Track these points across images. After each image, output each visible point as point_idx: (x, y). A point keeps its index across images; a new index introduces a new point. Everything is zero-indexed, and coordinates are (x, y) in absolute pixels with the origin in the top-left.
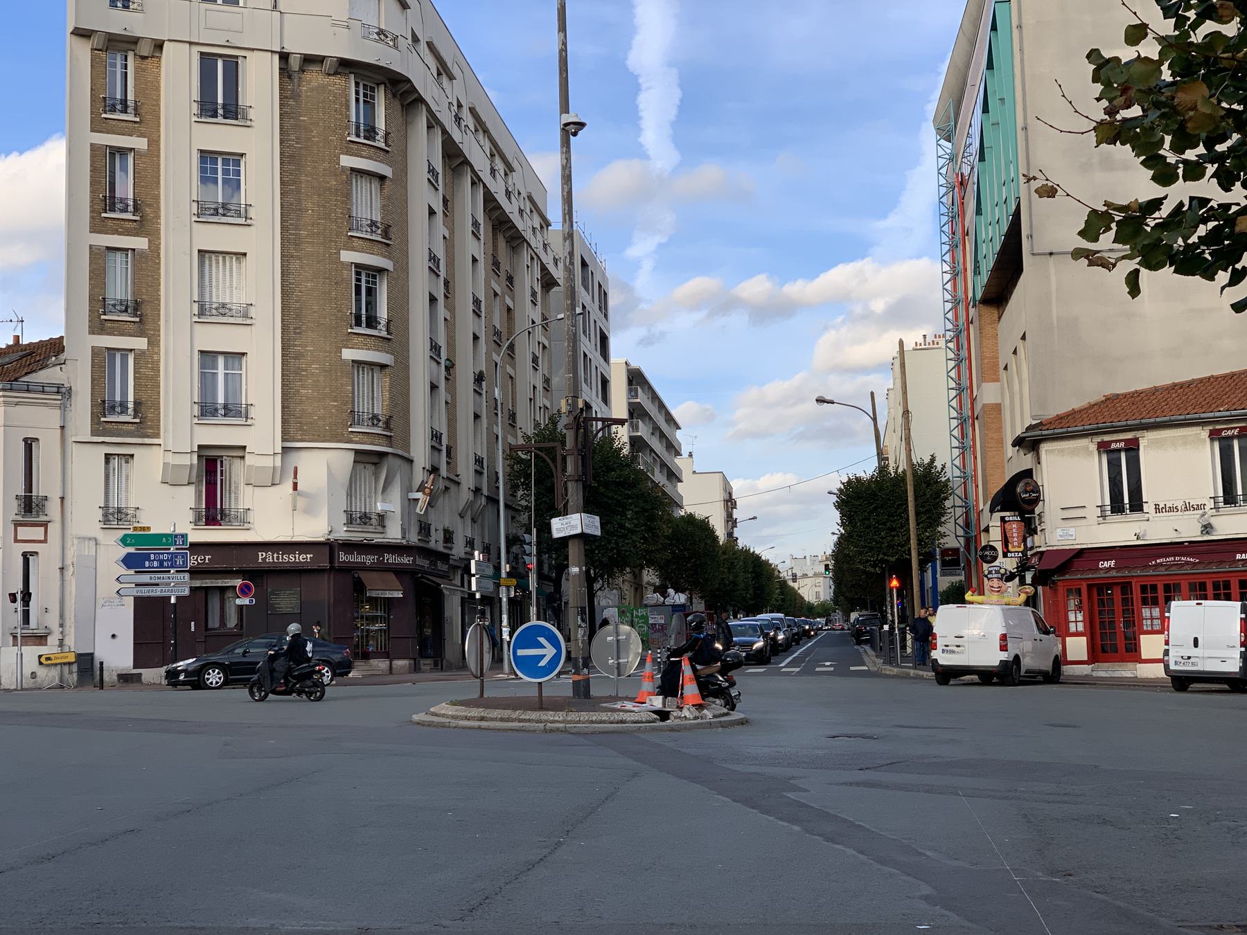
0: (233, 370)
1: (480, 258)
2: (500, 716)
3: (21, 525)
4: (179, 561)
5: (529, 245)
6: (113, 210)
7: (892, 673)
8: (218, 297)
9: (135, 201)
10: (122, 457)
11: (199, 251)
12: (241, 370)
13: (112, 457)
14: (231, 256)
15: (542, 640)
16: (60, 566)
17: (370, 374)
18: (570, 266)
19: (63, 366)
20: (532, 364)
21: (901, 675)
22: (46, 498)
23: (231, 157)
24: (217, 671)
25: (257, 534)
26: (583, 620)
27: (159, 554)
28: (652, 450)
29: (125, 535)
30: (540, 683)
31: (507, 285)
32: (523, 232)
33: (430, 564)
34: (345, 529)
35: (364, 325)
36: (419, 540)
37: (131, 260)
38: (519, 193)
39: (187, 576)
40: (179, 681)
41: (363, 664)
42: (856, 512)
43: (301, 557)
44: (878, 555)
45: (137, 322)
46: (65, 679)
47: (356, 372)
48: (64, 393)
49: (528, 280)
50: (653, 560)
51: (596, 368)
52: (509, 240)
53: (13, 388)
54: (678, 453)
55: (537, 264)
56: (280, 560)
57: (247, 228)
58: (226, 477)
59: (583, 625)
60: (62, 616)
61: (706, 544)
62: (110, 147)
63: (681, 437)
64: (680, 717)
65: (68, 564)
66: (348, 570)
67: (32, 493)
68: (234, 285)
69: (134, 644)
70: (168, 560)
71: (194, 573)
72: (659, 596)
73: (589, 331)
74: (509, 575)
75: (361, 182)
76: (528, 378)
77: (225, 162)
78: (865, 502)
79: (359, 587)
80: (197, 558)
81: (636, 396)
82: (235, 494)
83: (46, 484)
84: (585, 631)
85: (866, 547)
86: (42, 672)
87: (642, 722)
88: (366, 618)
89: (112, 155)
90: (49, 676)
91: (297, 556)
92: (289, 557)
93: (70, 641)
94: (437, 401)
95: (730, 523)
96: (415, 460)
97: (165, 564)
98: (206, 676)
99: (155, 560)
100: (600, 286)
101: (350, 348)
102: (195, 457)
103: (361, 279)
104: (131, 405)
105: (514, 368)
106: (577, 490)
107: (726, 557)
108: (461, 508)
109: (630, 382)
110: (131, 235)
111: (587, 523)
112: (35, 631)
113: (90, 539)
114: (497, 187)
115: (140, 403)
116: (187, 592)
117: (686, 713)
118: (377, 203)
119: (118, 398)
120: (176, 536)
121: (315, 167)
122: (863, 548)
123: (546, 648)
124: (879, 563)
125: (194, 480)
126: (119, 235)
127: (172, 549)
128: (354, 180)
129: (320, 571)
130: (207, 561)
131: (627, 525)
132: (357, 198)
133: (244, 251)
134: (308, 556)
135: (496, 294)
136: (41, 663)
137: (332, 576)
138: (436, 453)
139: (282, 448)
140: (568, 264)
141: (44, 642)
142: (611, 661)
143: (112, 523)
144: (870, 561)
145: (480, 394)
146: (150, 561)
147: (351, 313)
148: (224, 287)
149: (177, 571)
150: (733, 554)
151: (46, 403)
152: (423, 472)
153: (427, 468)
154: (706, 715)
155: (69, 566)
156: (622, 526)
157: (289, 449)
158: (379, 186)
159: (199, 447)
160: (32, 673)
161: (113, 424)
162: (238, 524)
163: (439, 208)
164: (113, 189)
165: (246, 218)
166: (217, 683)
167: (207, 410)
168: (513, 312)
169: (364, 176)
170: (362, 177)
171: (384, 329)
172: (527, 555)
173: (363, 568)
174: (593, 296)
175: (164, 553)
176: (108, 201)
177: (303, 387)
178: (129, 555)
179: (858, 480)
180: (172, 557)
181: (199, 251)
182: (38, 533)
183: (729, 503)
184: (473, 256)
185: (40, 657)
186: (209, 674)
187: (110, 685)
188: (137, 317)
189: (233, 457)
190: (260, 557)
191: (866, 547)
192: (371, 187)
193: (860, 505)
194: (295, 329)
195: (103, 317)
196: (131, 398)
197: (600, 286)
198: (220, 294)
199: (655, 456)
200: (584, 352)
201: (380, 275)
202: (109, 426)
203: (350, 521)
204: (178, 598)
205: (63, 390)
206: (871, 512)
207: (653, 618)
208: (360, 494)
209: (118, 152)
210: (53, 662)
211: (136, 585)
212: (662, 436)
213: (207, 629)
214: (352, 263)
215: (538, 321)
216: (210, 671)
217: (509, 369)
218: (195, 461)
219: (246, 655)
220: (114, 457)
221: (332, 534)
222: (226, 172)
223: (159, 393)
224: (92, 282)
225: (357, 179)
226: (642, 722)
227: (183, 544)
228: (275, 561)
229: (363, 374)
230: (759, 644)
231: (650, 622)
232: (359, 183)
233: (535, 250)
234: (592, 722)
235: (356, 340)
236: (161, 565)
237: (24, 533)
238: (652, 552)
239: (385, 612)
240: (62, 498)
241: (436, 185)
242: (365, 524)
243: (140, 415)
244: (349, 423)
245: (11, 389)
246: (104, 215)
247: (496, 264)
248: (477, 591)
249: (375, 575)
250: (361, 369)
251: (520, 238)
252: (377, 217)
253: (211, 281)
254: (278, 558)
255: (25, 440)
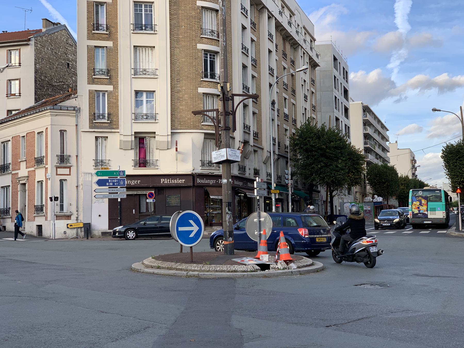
0: (150, 99)
1: (273, 50)
2: (167, 266)
3: (59, 168)
4: (122, 183)
5: (302, 47)
6: (98, 29)
7: (455, 235)
8: (143, 66)
9: (107, 25)
10: (103, 138)
11: (134, 46)
12: (153, 98)
13: (98, 138)
14: (148, 48)
15: (191, 221)
16: (76, 185)
17: (212, 99)
18: (222, 7)
19: (76, 98)
20: (304, 99)
21: (459, 236)
22: (70, 156)
23: (148, 4)
24: (132, 232)
25: (161, 171)
26: (229, 210)
27: (113, 179)
28: (374, 139)
29: (98, 171)
30: (191, 247)
31: (291, 64)
32: (298, 41)
33: (243, 184)
34: (201, 168)
35: (209, 77)
36: (239, 173)
37: (106, 52)
38: (298, 25)
39: (125, 189)
40: (116, 236)
41: (210, 228)
42: (450, 160)
43: (180, 181)
44: (461, 179)
45: (108, 79)
46: (79, 235)
47: (205, 98)
48: (77, 110)
49: (302, 65)
50: (357, 182)
51: (342, 103)
52: (293, 45)
53: (54, 108)
54: (387, 140)
55: (307, 56)
56: (171, 182)
57: (155, 35)
58: (147, 146)
59: (229, 212)
60: (77, 207)
61: (392, 176)
62: (96, 2)
63: (388, 134)
64: (275, 268)
65: (80, 184)
66: (201, 186)
67: (64, 154)
68: (150, 61)
69: (109, 219)
70: (116, 182)
71: (129, 188)
72: (370, 198)
73: (338, 87)
74: (276, 188)
75: (207, 13)
76: (301, 104)
77: (146, 6)
78: (454, 155)
79: (207, 194)
80: (134, 181)
81: (366, 117)
82: (152, 153)
83: (70, 150)
84: (230, 216)
85: (455, 175)
86: (68, 231)
87: (247, 271)
88: (212, 208)
89: (97, 6)
90: (72, 233)
91: (178, 180)
92: (174, 181)
93: (81, 218)
94: (248, 111)
95: (414, 169)
96: (235, 137)
97: (115, 184)
98: (128, 234)
99: (111, 182)
100: (344, 69)
101: (202, 87)
102: (133, 137)
103: (207, 57)
104: (106, 115)
105: (295, 100)
106: (226, 135)
107: (405, 182)
108: (264, 159)
109: (364, 111)
110: (105, 41)
111: (231, 154)
112: (65, 214)
113: (89, 174)
114: (284, 21)
115: (110, 114)
116: (125, 197)
117: (279, 266)
118: (215, 23)
119: (101, 112)
120: (120, 172)
121: (185, 7)
122: (453, 176)
123: (193, 226)
124: (462, 183)
125: (133, 147)
126: (100, 40)
127: (118, 177)
128: (204, 12)
129: (189, 187)
130: (139, 183)
131: (339, 166)
132: (205, 20)
133: (154, 46)
134: (183, 180)
135: (285, 68)
136: (68, 227)
137: (194, 189)
138: (247, 135)
139: (171, 132)
140: (221, 6)
141: (69, 218)
142: (256, 233)
143: (99, 166)
144: (457, 182)
145: (274, 110)
146: (109, 183)
147: (202, 72)
148: (146, 62)
149: (121, 187)
150: (408, 181)
151: (69, 115)
152: (240, 143)
153: (241, 141)
154: (291, 267)
155: (80, 185)
156: (337, 167)
157: (174, 133)
158: (215, 15)
159: (135, 133)
160: (64, 232)
161: (99, 123)
162: (154, 166)
163: (248, 25)
164: (97, 20)
165: (154, 31)
166: (132, 237)
167: (137, 117)
168: (294, 77)
169: (208, 10)
170: (207, 10)
171: (218, 79)
172: (287, 179)
173: (209, 186)
174: (340, 73)
175: (115, 179)
176: (95, 26)
177: (181, 105)
178: (99, 180)
179: (452, 145)
180: (118, 181)
181: (134, 46)
182: (66, 171)
183: (413, 161)
184: (269, 49)
185: (67, 225)
186: (129, 233)
187: (98, 237)
188: (108, 76)
189: (151, 137)
190: (162, 181)
191: (455, 175)
192: (212, 15)
193: (452, 156)
194: (177, 79)
195: (94, 77)
196: (106, 112)
197: (344, 69)
198: (143, 65)
199: (376, 141)
200: (335, 96)
201: (216, 55)
202: (97, 124)
203: (203, 165)
204: (121, 199)
205: (76, 109)
206: (457, 159)
207: (365, 207)
208: (208, 153)
209: (100, 4)
210: (73, 227)
211: (109, 193)
212: (379, 133)
213: (140, 212)
214: (202, 49)
215: (308, 81)
216: (129, 232)
217: (292, 101)
218: (133, 139)
219: (145, 224)
220: (99, 138)
221: (194, 171)
222: (146, 11)
223: (118, 110)
224: (88, 62)
225: (205, 11)
226: (247, 271)
227: (123, 175)
228: (168, 182)
229: (209, 99)
230: (397, 220)
231: (364, 209)
232: (206, 14)
233: (305, 49)
234: (217, 271)
235: (204, 84)
236: (114, 185)
237: (60, 171)
238: (357, 179)
239: (219, 205)
240: (77, 156)
241: (246, 16)
242: (211, 166)
243: (110, 119)
244: (202, 121)
245: (53, 109)
246: (93, 32)
247: (285, 55)
248: (257, 195)
249: (214, 189)
250: (207, 97)
251: (297, 44)
252: (215, 29)
253: (140, 60)
254: (169, 181)
255: (61, 131)
